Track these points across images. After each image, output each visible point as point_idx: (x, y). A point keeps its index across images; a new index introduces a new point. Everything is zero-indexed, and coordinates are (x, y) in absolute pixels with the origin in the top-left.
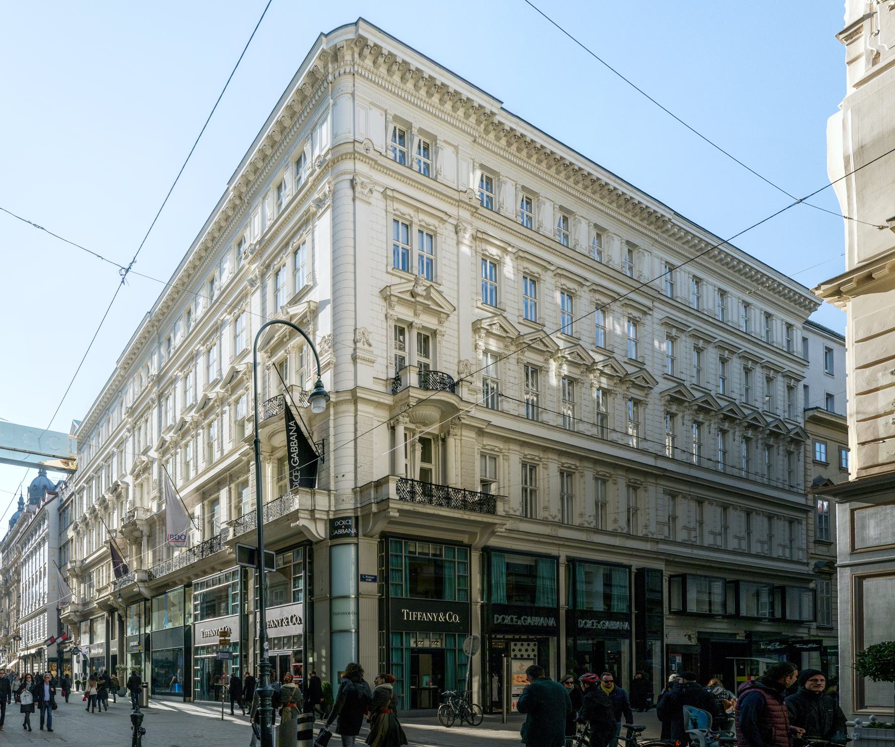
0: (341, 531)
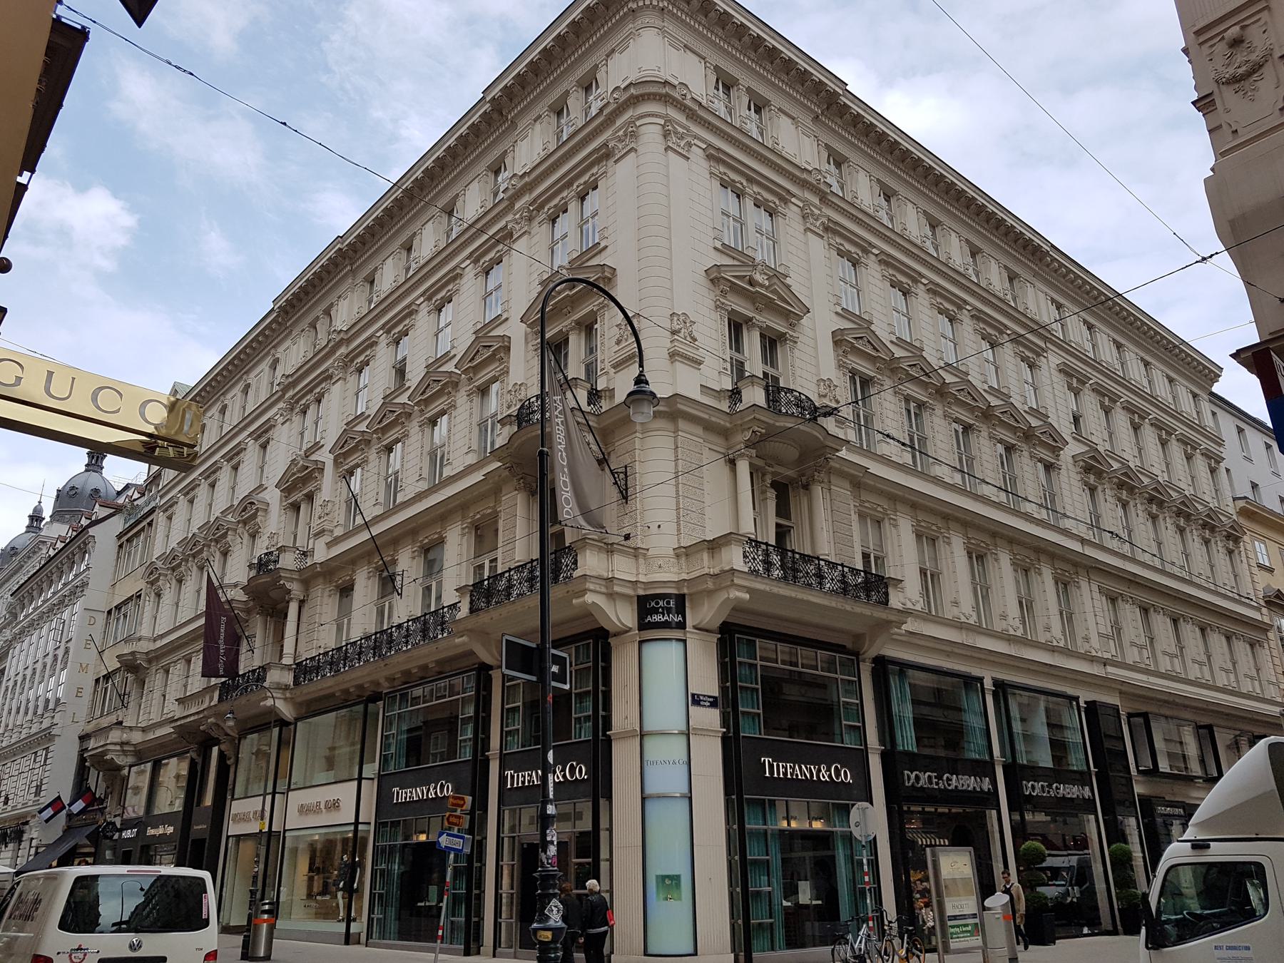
0: (657, 618)
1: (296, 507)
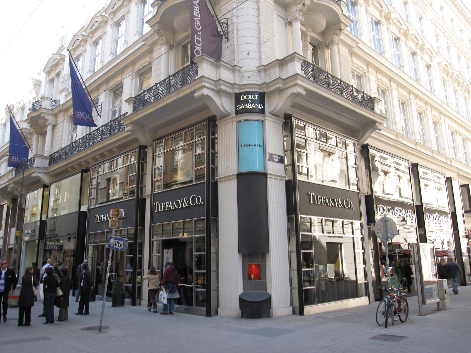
1: (52, 81)
